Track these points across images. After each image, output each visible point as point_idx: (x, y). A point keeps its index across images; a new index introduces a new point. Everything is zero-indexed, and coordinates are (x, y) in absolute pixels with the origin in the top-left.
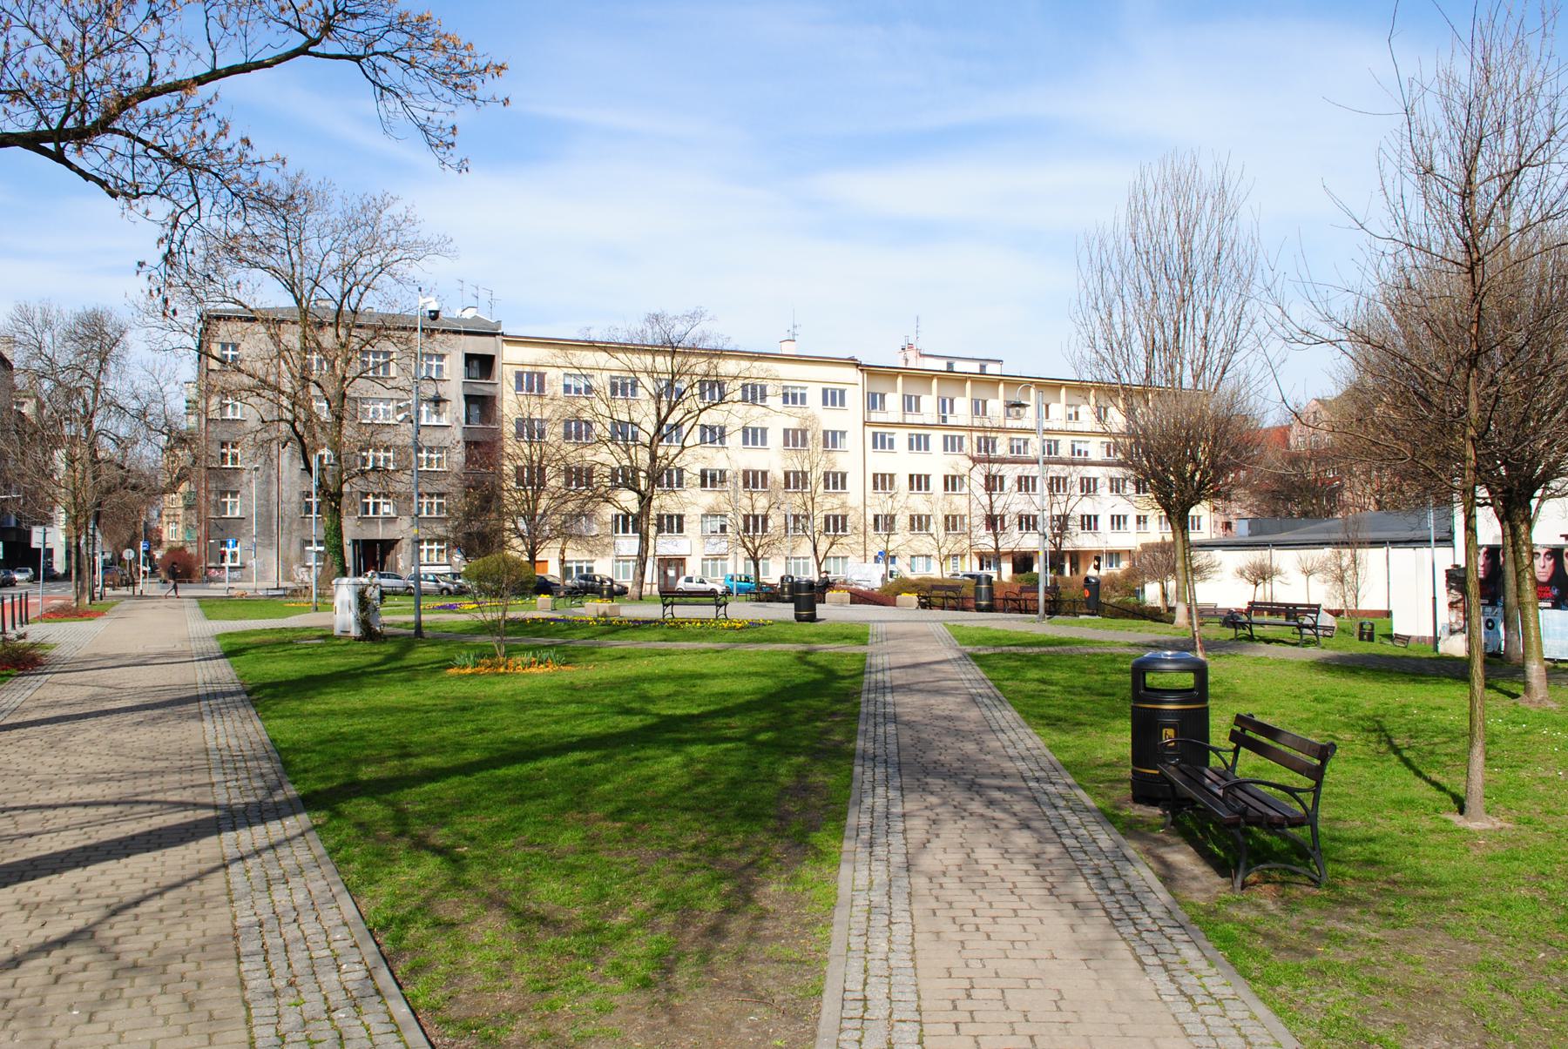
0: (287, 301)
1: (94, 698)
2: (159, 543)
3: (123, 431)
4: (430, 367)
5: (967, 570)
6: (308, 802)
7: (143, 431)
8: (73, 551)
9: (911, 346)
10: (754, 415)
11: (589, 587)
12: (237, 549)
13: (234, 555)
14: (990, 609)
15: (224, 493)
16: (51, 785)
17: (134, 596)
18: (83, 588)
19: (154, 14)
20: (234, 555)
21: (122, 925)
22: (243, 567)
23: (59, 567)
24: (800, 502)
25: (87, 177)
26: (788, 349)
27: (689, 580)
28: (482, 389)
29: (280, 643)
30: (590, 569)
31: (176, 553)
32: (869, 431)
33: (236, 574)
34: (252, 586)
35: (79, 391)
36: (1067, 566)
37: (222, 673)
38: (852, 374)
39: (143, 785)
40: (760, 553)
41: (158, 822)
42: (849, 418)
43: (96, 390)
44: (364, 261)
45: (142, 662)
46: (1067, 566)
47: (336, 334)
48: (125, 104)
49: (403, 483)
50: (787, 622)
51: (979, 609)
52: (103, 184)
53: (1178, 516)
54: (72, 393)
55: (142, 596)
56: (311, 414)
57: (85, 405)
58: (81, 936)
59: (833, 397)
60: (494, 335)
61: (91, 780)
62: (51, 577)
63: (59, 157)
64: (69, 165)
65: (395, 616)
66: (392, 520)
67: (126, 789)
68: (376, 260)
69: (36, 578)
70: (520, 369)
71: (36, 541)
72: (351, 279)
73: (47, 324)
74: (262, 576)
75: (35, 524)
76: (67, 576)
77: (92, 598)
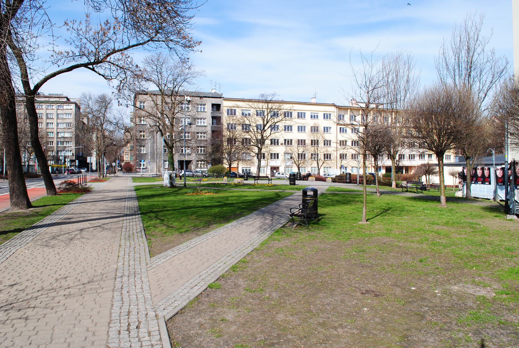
0: (158, 89)
1: (102, 198)
2: (123, 161)
3: (111, 129)
4: (201, 108)
5: (370, 172)
6: (141, 214)
7: (117, 128)
8: (98, 163)
9: (354, 99)
10: (301, 122)
11: (247, 175)
12: (145, 163)
13: (144, 165)
14: (350, 183)
15: (141, 146)
16: (94, 210)
17: (115, 176)
18: (101, 174)
19: (115, 33)
20: (144, 165)
21: (104, 225)
22: (146, 168)
23: (94, 168)
24: (313, 150)
25: (100, 74)
26: (313, 101)
27: (279, 174)
28: (217, 114)
29: (150, 188)
30: (250, 170)
31: (128, 164)
32: (339, 127)
33: (144, 170)
34: (147, 175)
35: (99, 118)
36: (404, 171)
37: (134, 194)
38: (333, 109)
39: (111, 211)
40: (300, 166)
41: (113, 215)
42: (330, 123)
43: (104, 117)
44: (179, 78)
45: (114, 191)
46: (404, 171)
47: (172, 97)
48: (108, 55)
49: (193, 144)
50: (288, 185)
51: (347, 183)
52: (103, 76)
53: (440, 155)
54: (98, 118)
55: (117, 176)
56: (164, 124)
57: (101, 122)
58: (100, 226)
59: (327, 116)
60: (220, 98)
61: (102, 210)
62: (92, 171)
63: (93, 70)
64: (96, 72)
65: (179, 182)
66: (190, 154)
67: (108, 211)
68: (182, 78)
69: (88, 171)
70: (229, 108)
71: (88, 161)
72: (175, 84)
73: (90, 98)
74: (152, 171)
75: (88, 156)
76: (96, 171)
77: (103, 177)
